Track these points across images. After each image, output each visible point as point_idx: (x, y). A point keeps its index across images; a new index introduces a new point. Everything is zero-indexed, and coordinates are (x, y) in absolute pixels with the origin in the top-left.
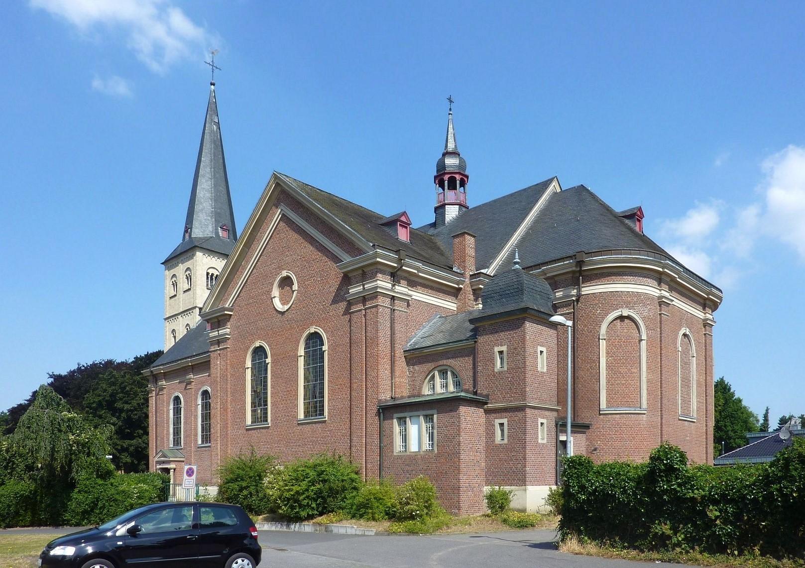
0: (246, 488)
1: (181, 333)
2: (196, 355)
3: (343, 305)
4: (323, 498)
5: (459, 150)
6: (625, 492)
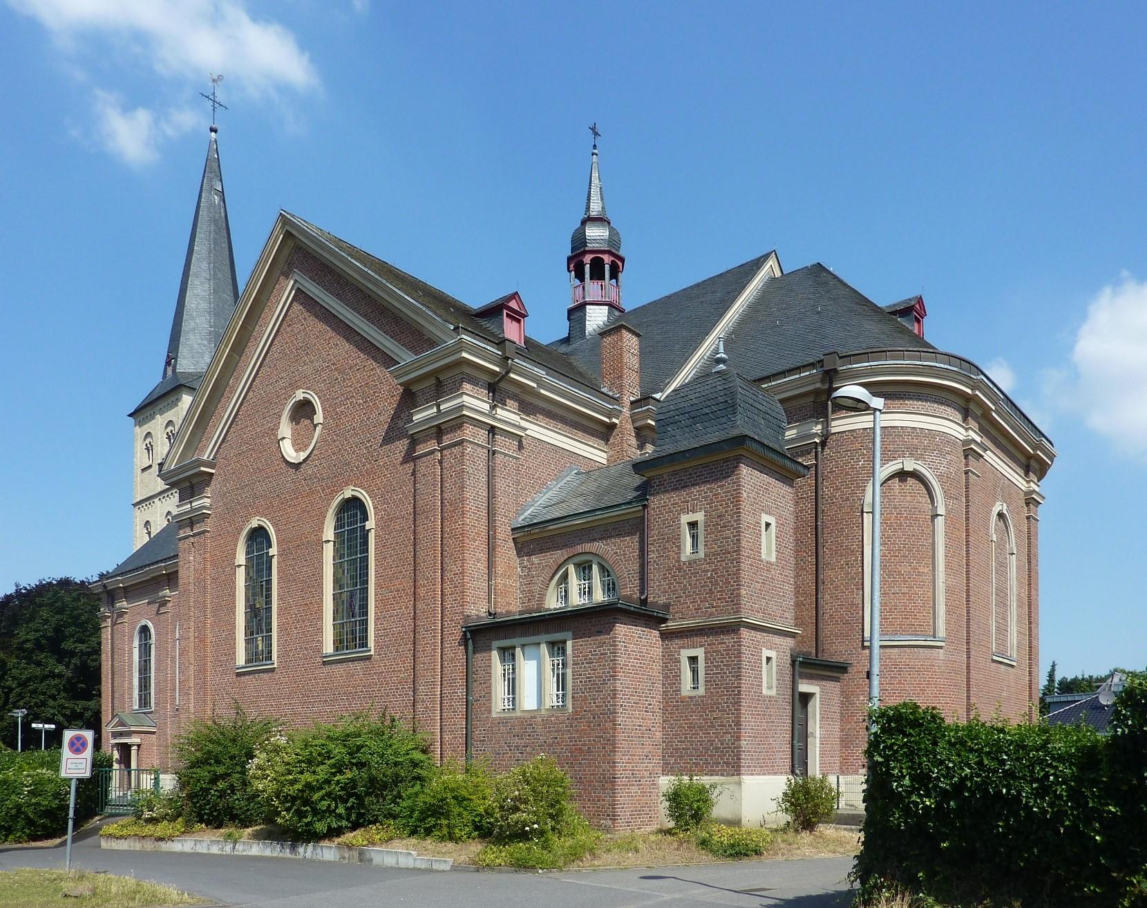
0: (224, 776)
1: (159, 524)
3: (402, 445)
4: (358, 797)
5: (609, 216)
6: (1044, 790)
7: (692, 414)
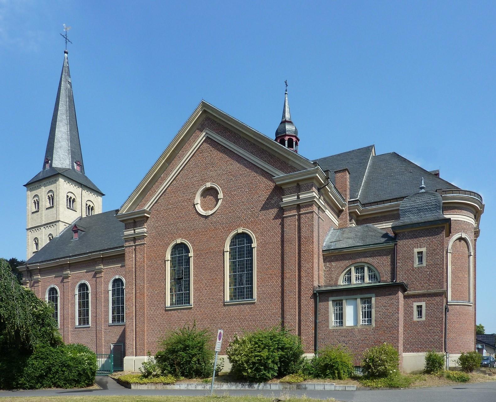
1: (44, 242)
2: (73, 256)
5: (292, 121)
7: (419, 208)
